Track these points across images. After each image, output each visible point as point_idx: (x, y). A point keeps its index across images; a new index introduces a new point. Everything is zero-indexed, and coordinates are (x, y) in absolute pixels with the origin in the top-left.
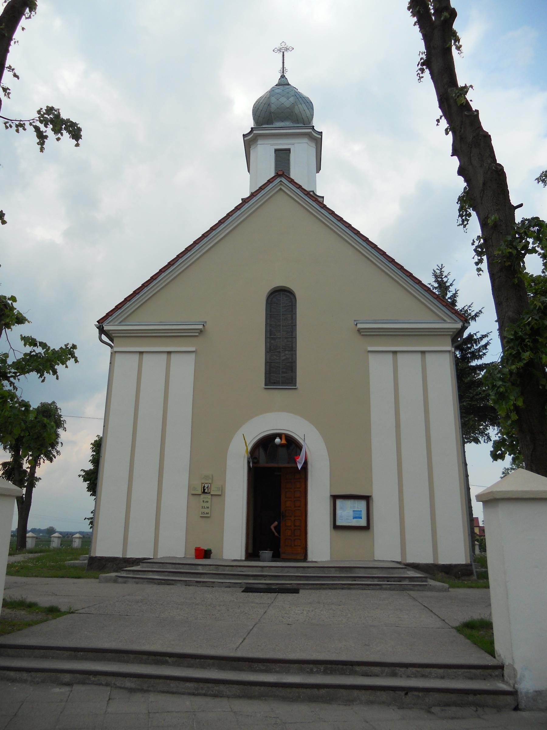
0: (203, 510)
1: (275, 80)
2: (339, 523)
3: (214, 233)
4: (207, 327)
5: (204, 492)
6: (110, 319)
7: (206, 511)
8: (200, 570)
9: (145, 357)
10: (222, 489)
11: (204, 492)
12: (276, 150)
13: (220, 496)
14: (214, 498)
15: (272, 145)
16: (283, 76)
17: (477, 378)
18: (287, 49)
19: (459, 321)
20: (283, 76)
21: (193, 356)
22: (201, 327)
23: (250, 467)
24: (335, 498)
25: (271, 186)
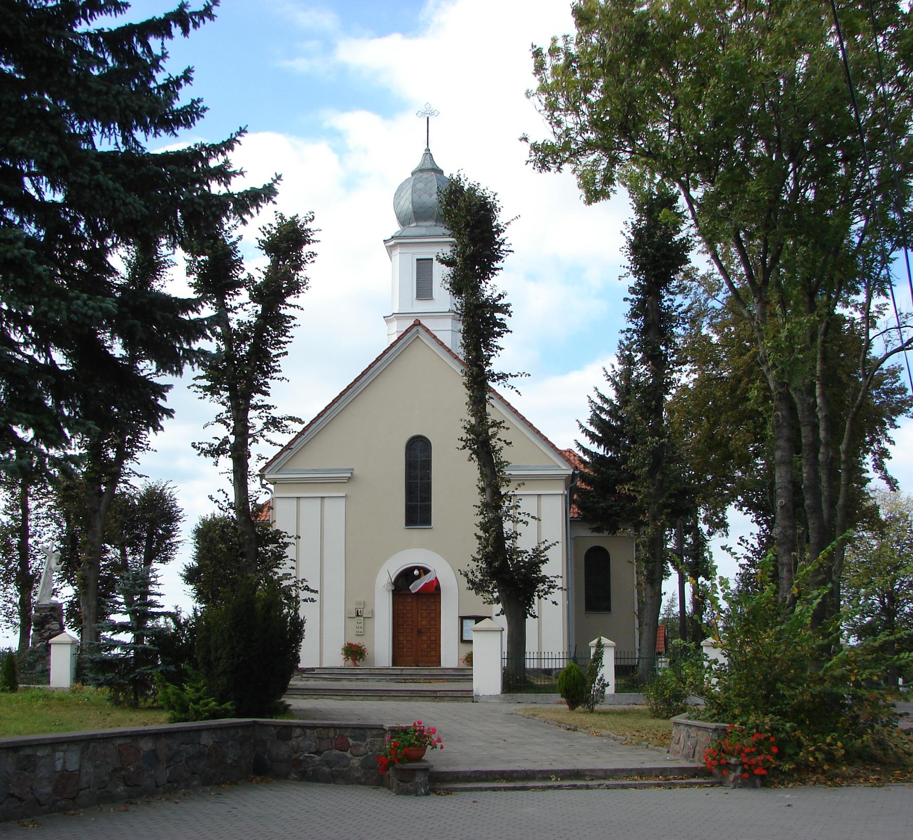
0: (358, 630)
1: (416, 161)
2: (465, 638)
3: (358, 384)
4: (355, 472)
5: (358, 615)
6: (270, 468)
7: (362, 630)
8: (358, 671)
9: (302, 501)
10: (373, 612)
11: (358, 615)
12: (417, 260)
13: (372, 617)
14: (366, 620)
15: (413, 254)
16: (428, 152)
17: (843, 457)
18: (432, 113)
19: (570, 468)
20: (428, 152)
21: (343, 500)
22: (349, 475)
23: (185, 311)
24: (462, 619)
25: (409, 334)
